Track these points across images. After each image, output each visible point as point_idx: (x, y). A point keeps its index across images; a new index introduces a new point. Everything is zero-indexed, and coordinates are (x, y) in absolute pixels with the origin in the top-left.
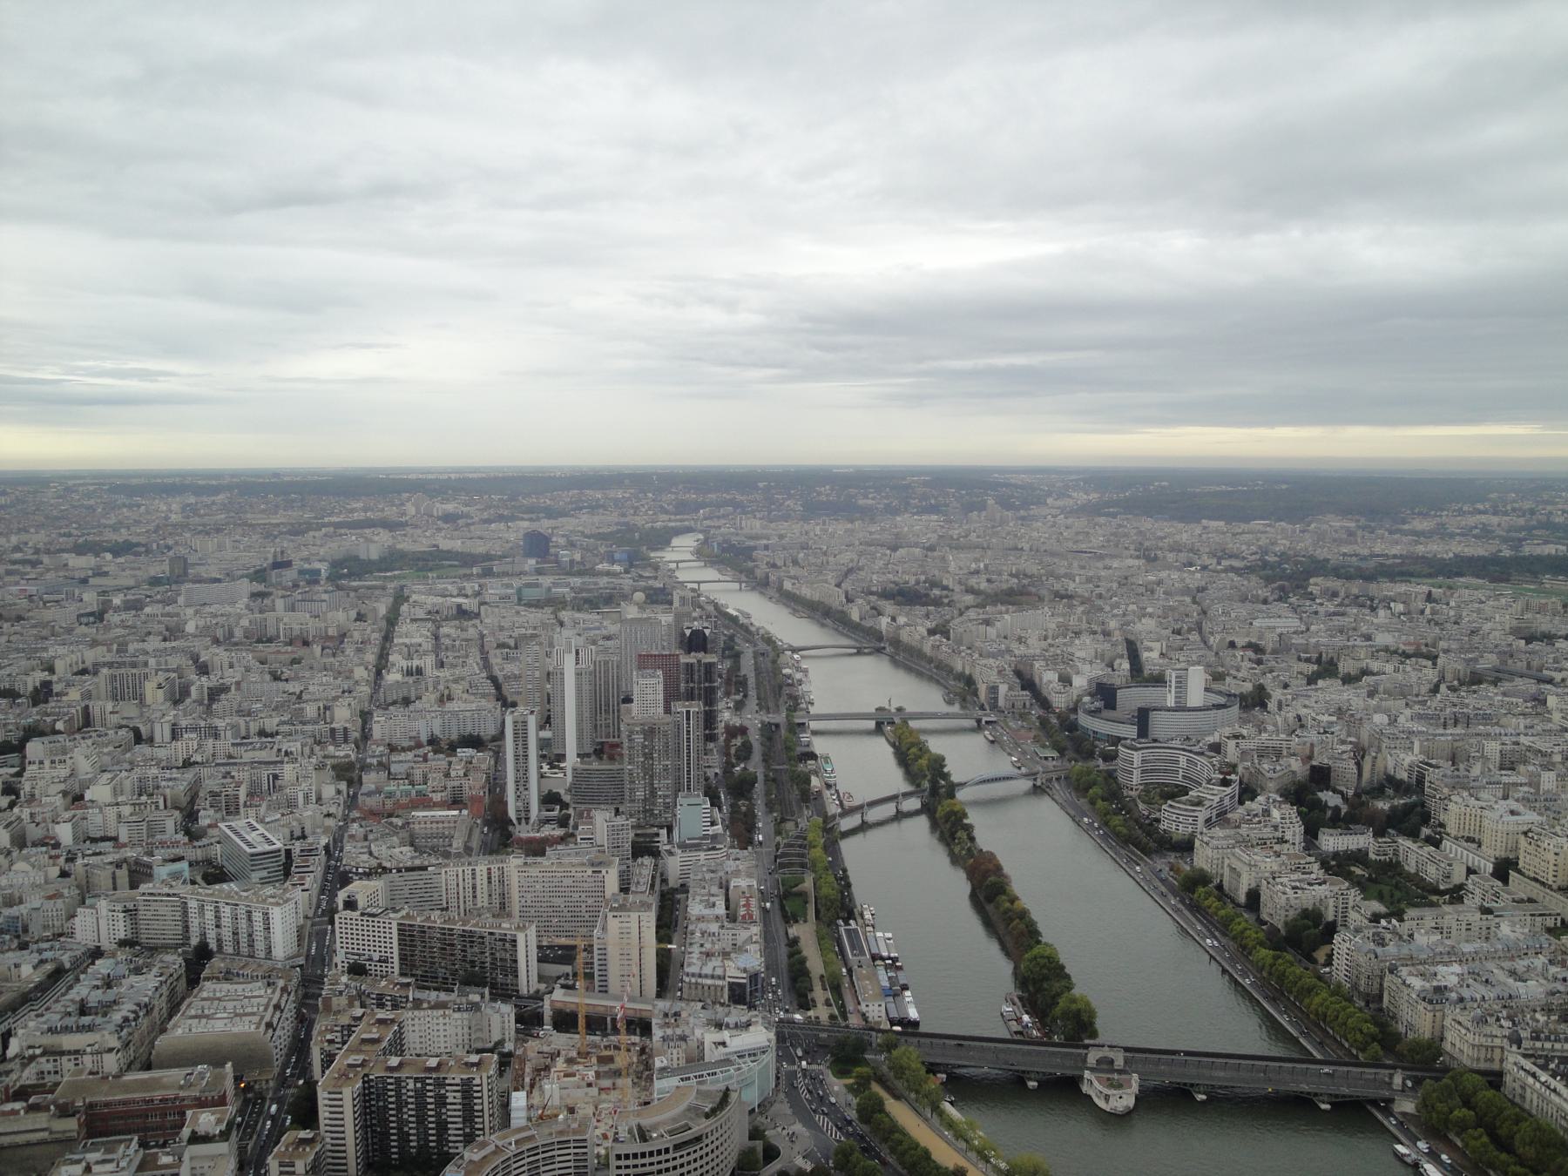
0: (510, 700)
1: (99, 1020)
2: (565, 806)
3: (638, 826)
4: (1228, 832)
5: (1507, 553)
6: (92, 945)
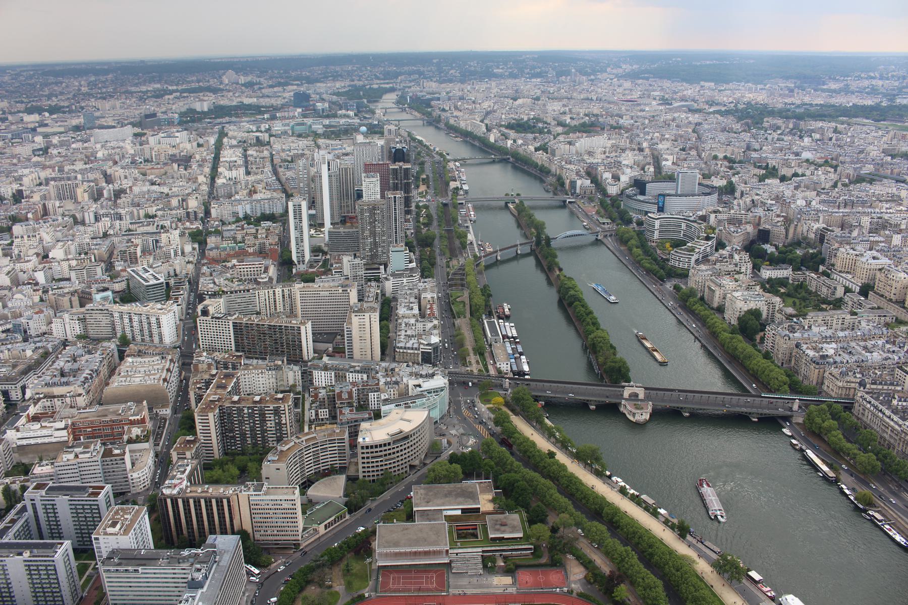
1: (72, 379)
2: (325, 253)
5: (884, 104)
6: (63, 338)
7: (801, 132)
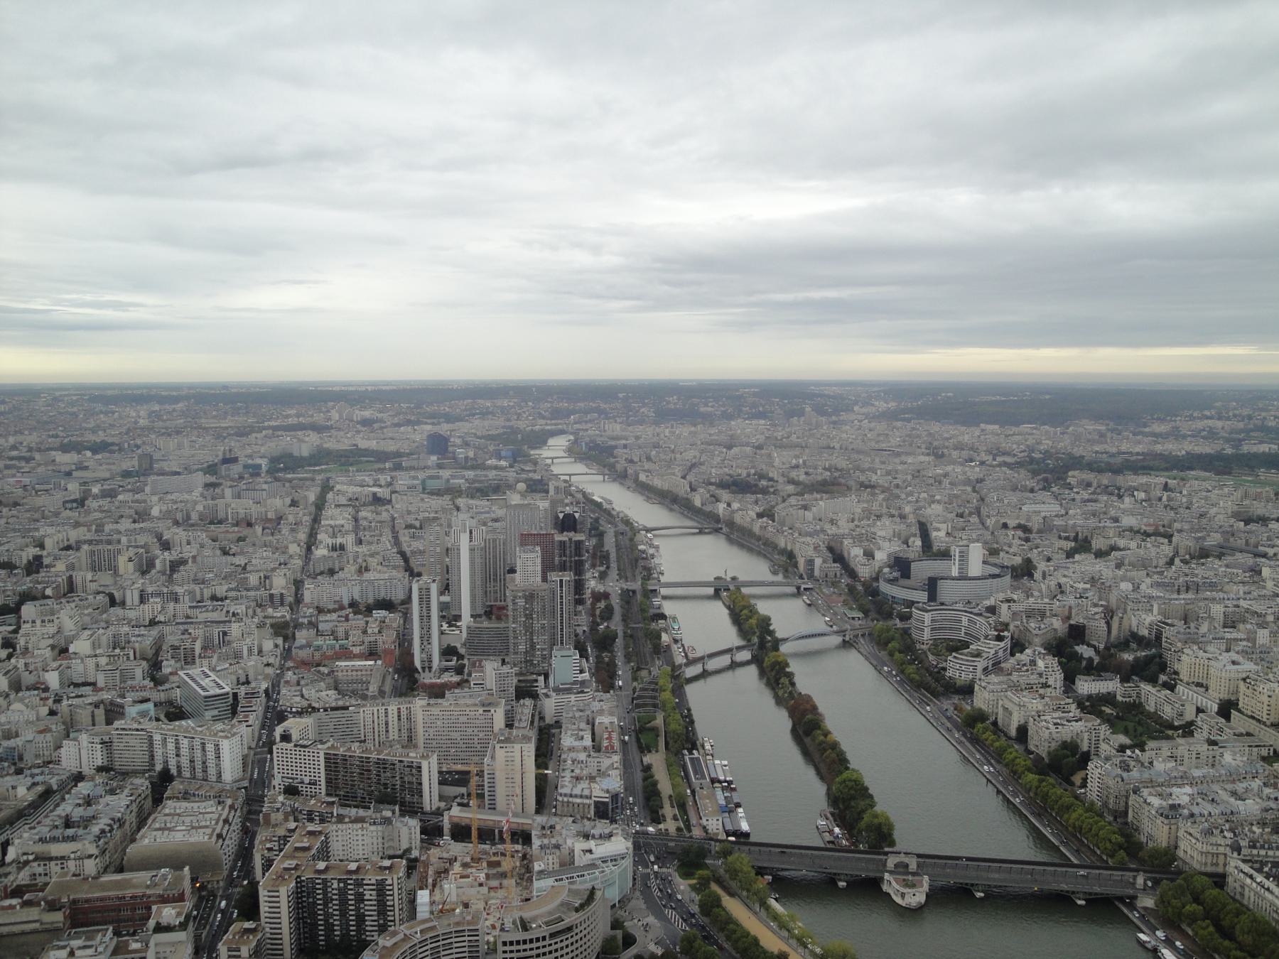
0: (416, 571)
1: (81, 832)
3: (520, 674)
4: (1001, 678)
5: (1229, 451)
6: (75, 770)
7: (1119, 489)
